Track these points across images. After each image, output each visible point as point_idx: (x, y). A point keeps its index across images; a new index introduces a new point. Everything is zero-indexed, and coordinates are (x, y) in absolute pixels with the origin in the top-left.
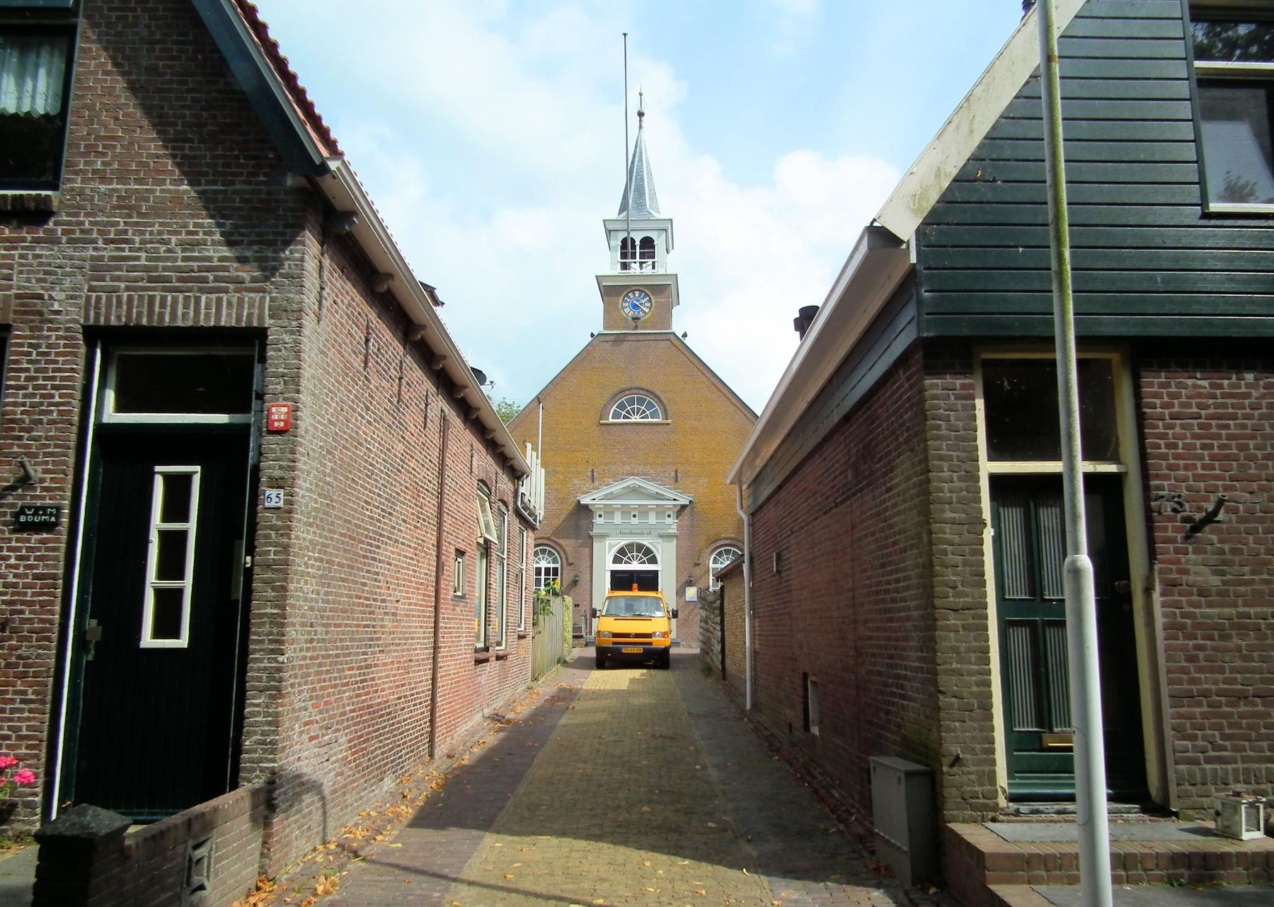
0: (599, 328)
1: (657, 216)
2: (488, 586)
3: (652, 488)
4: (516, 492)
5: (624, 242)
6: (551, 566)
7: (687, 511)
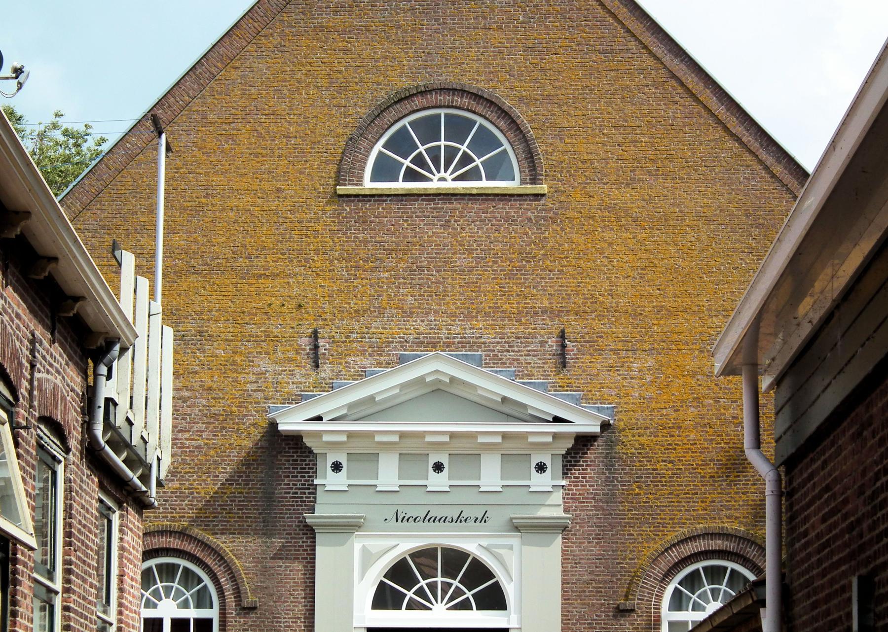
3: (492, 385)
7: (594, 453)
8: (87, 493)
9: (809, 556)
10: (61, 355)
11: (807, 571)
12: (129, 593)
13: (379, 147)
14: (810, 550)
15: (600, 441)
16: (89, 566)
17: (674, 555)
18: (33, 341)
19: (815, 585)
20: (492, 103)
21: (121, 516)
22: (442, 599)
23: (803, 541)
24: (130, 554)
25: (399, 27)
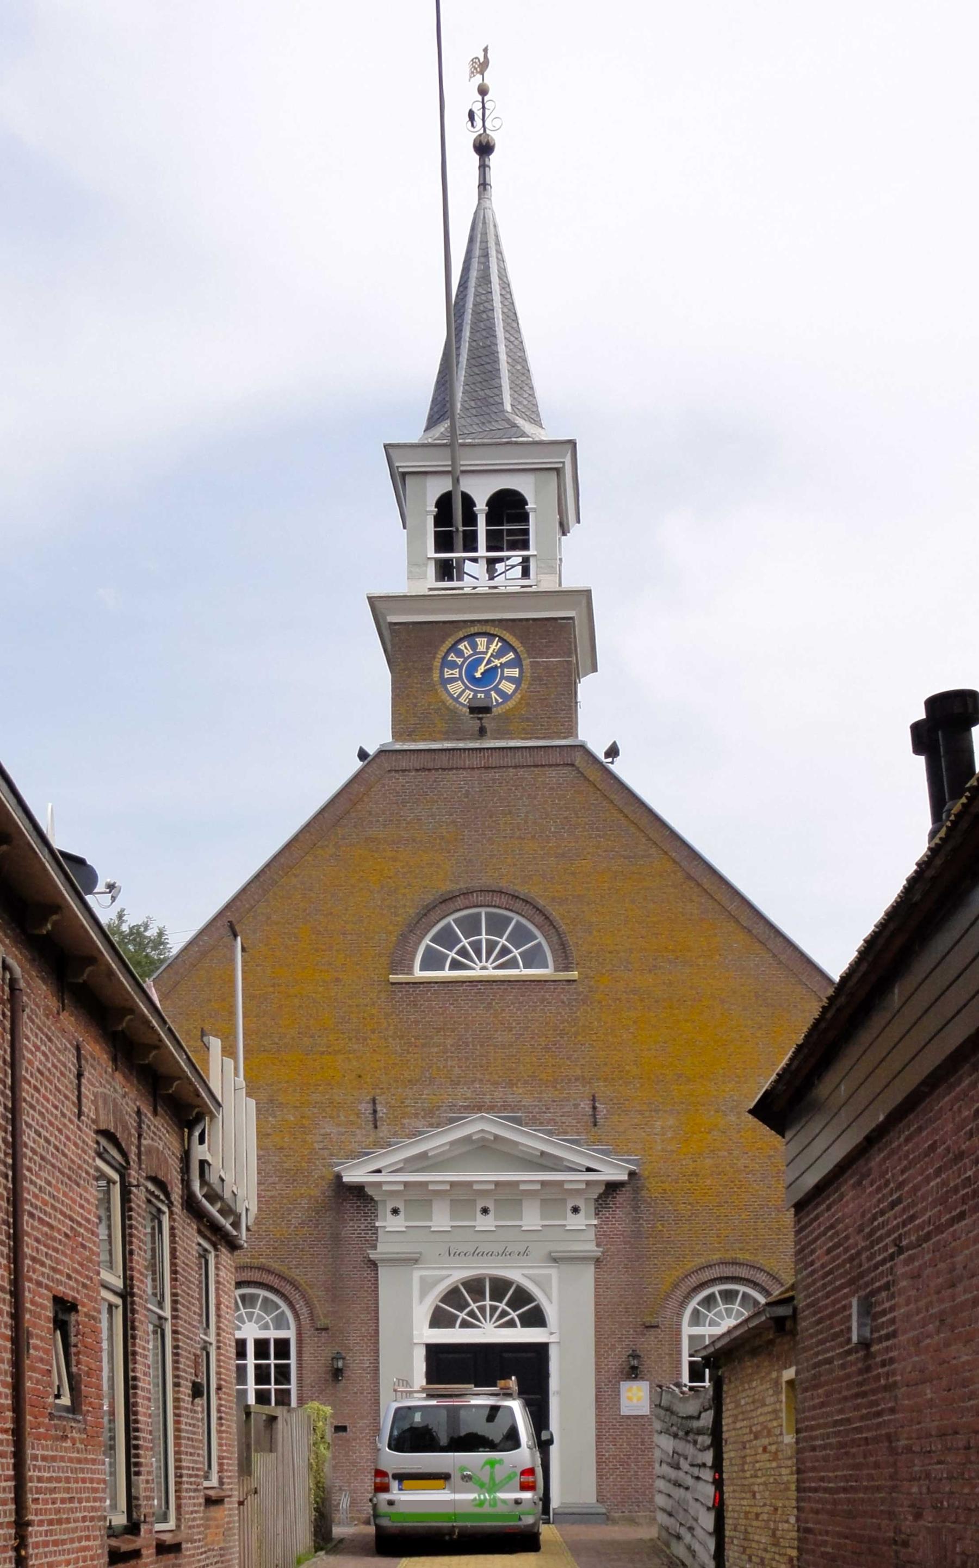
0: (378, 733)
1: (544, 436)
2: (130, 1384)
3: (531, 1141)
4: (186, 1158)
5: (444, 503)
6: (273, 1334)
7: (622, 1197)
8: (188, 1238)
9: (814, 1282)
10: (163, 1126)
11: (815, 1292)
12: (225, 1318)
13: (427, 941)
14: (816, 1276)
15: (628, 1188)
16: (192, 1297)
17: (694, 1281)
18: (139, 1113)
19: (821, 1304)
20: (527, 902)
21: (217, 1256)
22: (491, 1316)
23: (810, 1269)
24: (225, 1286)
25: (442, 838)
